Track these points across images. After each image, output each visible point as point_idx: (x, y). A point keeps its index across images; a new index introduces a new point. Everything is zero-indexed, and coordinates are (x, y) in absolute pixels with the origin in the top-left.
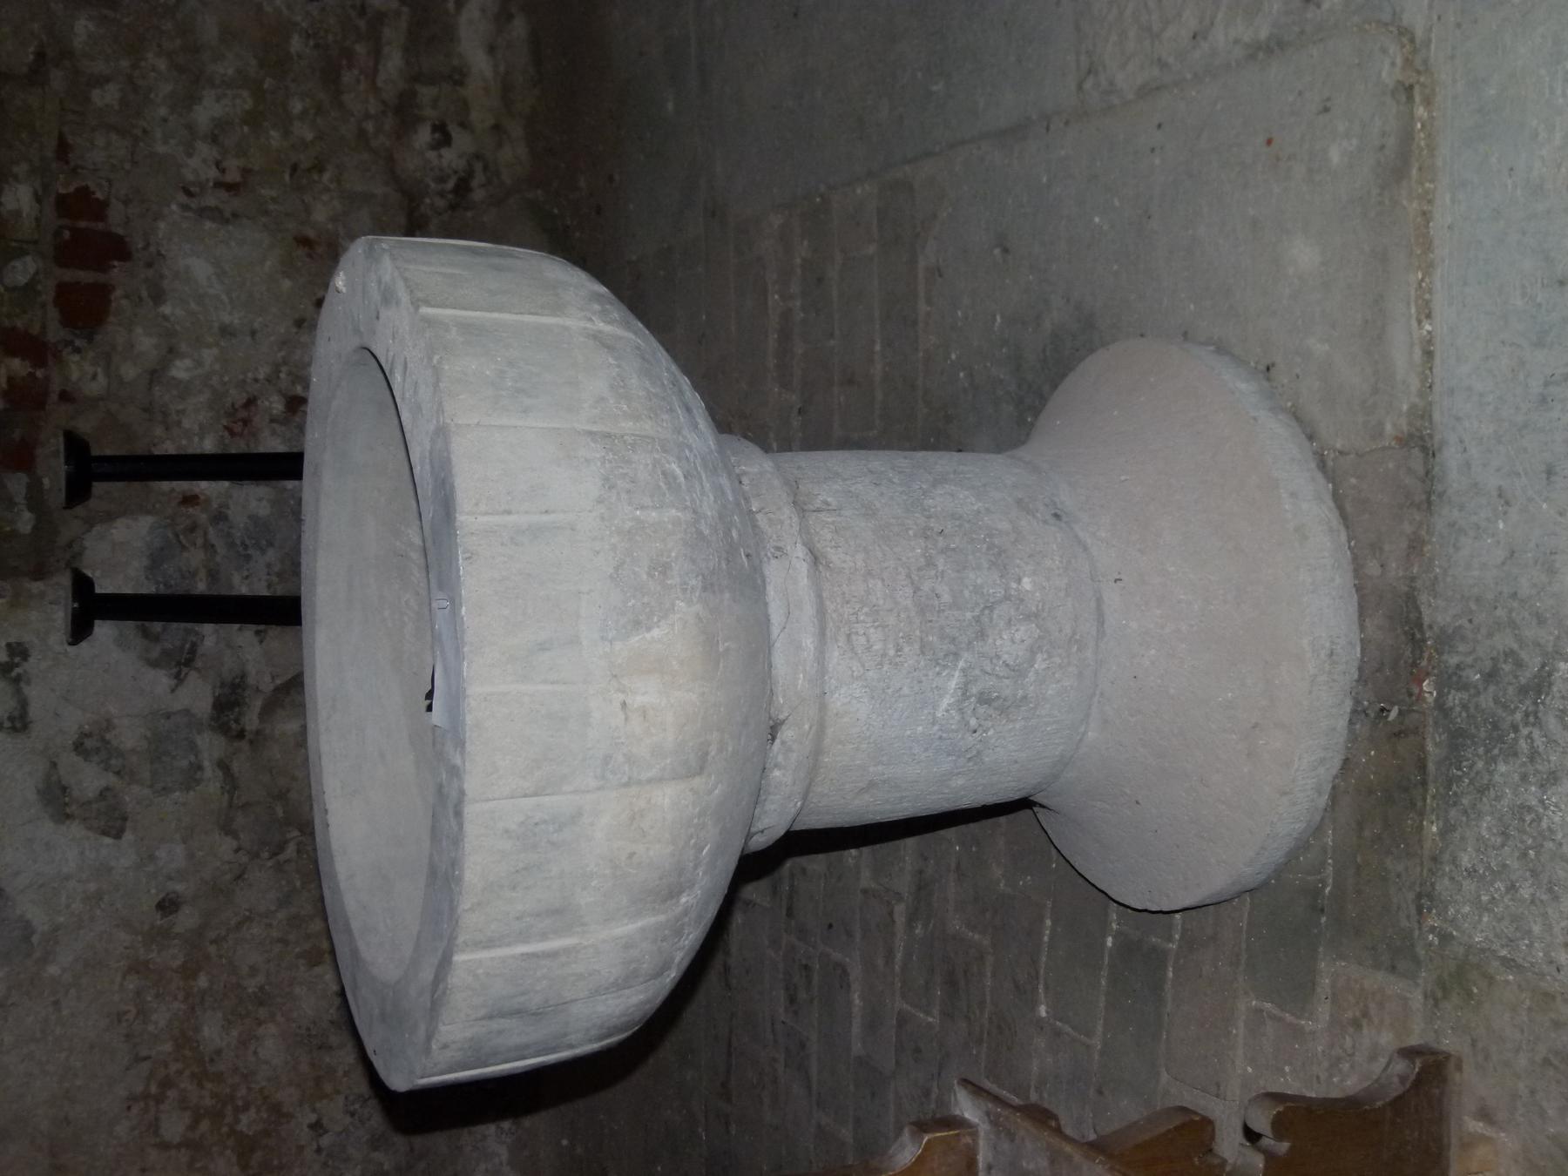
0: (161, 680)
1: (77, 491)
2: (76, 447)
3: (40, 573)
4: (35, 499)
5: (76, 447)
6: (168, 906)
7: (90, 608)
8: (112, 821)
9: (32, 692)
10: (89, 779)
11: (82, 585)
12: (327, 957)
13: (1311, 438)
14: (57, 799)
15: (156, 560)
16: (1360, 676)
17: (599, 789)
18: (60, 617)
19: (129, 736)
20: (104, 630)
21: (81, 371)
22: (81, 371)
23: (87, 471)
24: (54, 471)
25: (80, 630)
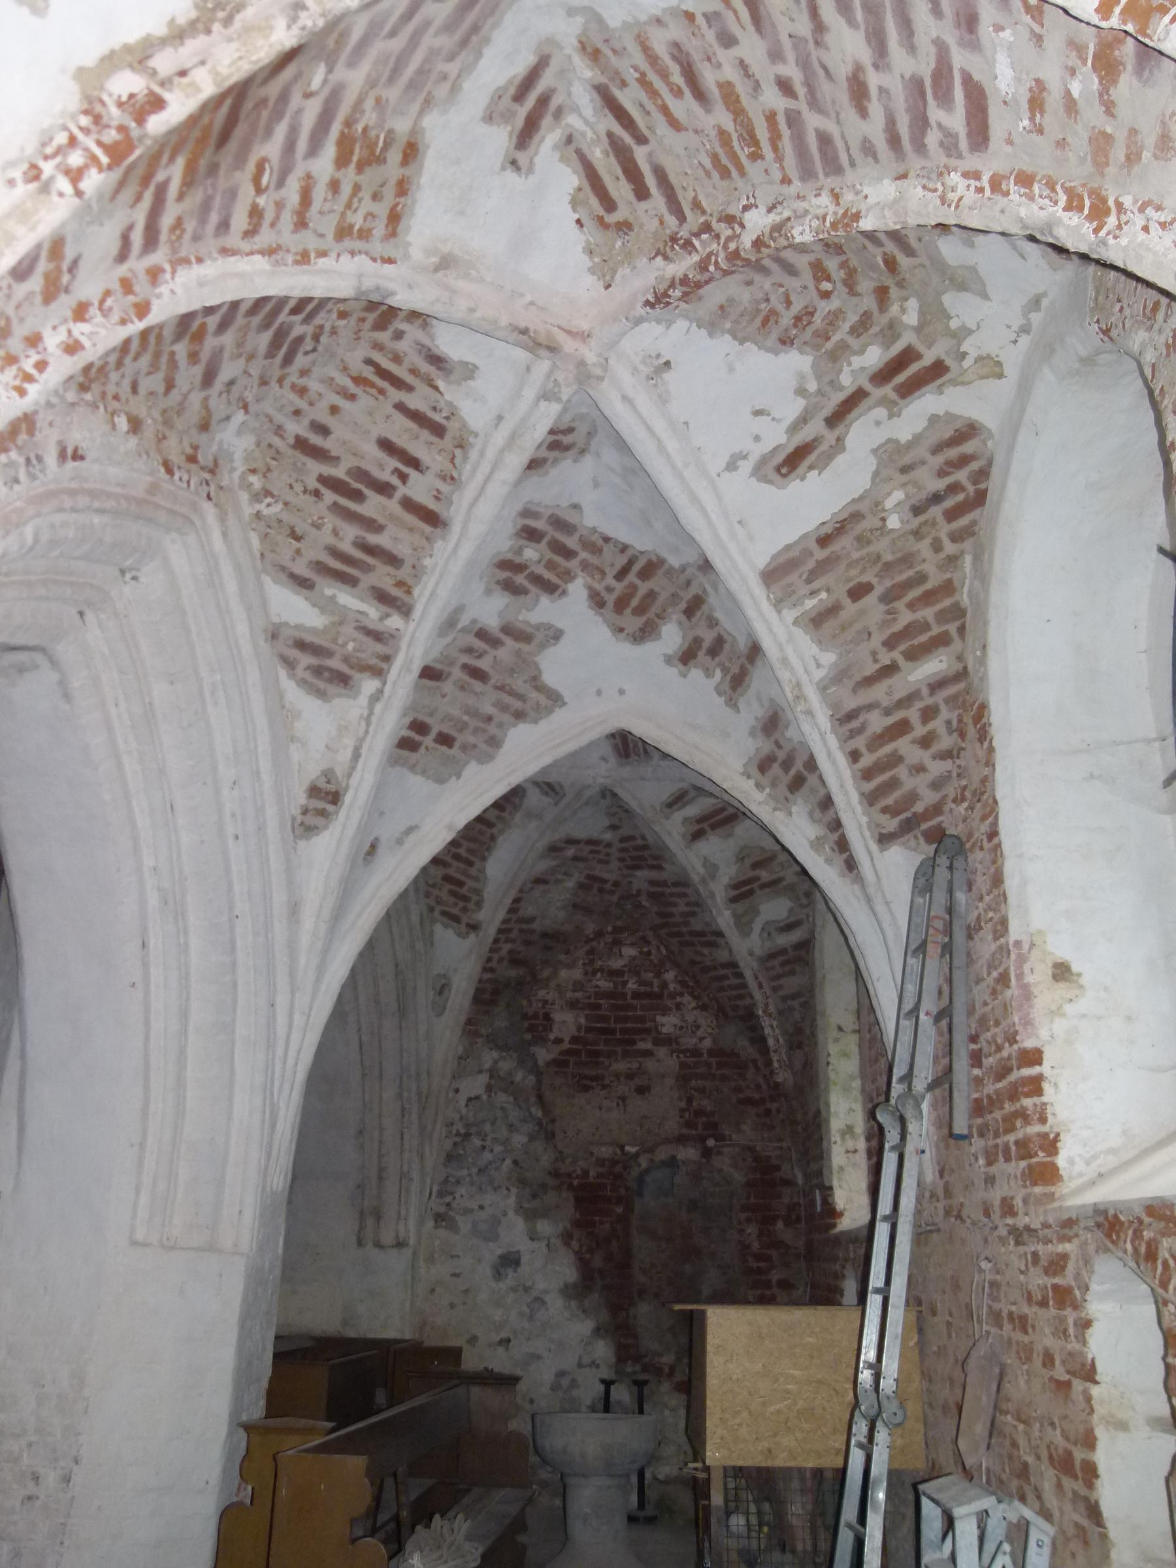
0: (588, 1402)
1: (635, 1382)
2: (644, 1383)
3: (616, 1373)
4: (634, 1373)
5: (644, 1383)
6: (532, 1401)
7: (607, 1384)
8: (555, 1387)
9: (588, 1370)
10: (565, 1382)
11: (612, 1382)
12: (955, 1411)
13: (1094, 1183)
14: (561, 1374)
15: (619, 1403)
16: (320, 608)
17: (1039, 1497)
18: (605, 1376)
19: (575, 1393)
20: (602, 1388)
21: (665, 1387)
22: (665, 1387)
23: (640, 1384)
24: (642, 1377)
25: (603, 1381)
